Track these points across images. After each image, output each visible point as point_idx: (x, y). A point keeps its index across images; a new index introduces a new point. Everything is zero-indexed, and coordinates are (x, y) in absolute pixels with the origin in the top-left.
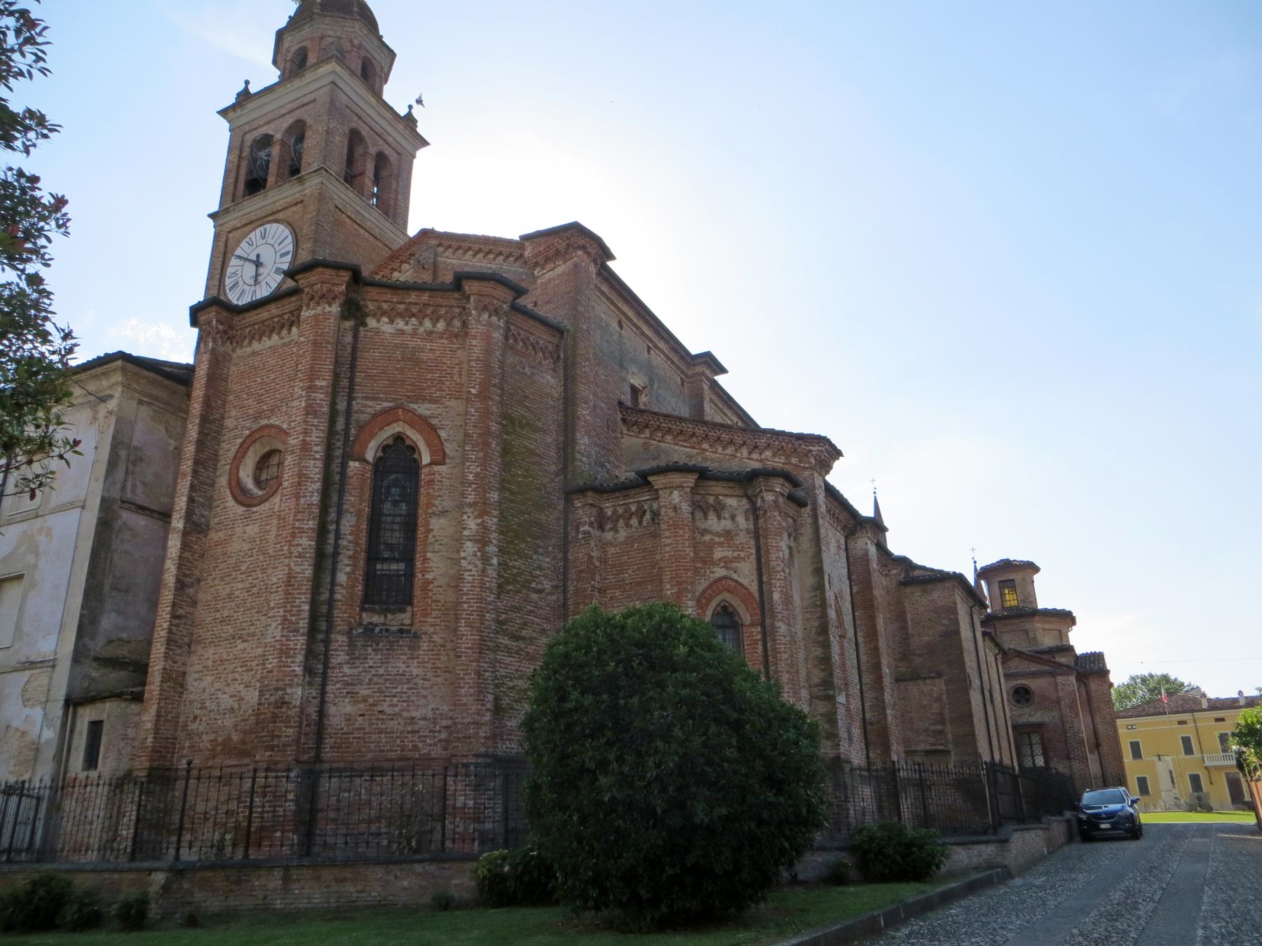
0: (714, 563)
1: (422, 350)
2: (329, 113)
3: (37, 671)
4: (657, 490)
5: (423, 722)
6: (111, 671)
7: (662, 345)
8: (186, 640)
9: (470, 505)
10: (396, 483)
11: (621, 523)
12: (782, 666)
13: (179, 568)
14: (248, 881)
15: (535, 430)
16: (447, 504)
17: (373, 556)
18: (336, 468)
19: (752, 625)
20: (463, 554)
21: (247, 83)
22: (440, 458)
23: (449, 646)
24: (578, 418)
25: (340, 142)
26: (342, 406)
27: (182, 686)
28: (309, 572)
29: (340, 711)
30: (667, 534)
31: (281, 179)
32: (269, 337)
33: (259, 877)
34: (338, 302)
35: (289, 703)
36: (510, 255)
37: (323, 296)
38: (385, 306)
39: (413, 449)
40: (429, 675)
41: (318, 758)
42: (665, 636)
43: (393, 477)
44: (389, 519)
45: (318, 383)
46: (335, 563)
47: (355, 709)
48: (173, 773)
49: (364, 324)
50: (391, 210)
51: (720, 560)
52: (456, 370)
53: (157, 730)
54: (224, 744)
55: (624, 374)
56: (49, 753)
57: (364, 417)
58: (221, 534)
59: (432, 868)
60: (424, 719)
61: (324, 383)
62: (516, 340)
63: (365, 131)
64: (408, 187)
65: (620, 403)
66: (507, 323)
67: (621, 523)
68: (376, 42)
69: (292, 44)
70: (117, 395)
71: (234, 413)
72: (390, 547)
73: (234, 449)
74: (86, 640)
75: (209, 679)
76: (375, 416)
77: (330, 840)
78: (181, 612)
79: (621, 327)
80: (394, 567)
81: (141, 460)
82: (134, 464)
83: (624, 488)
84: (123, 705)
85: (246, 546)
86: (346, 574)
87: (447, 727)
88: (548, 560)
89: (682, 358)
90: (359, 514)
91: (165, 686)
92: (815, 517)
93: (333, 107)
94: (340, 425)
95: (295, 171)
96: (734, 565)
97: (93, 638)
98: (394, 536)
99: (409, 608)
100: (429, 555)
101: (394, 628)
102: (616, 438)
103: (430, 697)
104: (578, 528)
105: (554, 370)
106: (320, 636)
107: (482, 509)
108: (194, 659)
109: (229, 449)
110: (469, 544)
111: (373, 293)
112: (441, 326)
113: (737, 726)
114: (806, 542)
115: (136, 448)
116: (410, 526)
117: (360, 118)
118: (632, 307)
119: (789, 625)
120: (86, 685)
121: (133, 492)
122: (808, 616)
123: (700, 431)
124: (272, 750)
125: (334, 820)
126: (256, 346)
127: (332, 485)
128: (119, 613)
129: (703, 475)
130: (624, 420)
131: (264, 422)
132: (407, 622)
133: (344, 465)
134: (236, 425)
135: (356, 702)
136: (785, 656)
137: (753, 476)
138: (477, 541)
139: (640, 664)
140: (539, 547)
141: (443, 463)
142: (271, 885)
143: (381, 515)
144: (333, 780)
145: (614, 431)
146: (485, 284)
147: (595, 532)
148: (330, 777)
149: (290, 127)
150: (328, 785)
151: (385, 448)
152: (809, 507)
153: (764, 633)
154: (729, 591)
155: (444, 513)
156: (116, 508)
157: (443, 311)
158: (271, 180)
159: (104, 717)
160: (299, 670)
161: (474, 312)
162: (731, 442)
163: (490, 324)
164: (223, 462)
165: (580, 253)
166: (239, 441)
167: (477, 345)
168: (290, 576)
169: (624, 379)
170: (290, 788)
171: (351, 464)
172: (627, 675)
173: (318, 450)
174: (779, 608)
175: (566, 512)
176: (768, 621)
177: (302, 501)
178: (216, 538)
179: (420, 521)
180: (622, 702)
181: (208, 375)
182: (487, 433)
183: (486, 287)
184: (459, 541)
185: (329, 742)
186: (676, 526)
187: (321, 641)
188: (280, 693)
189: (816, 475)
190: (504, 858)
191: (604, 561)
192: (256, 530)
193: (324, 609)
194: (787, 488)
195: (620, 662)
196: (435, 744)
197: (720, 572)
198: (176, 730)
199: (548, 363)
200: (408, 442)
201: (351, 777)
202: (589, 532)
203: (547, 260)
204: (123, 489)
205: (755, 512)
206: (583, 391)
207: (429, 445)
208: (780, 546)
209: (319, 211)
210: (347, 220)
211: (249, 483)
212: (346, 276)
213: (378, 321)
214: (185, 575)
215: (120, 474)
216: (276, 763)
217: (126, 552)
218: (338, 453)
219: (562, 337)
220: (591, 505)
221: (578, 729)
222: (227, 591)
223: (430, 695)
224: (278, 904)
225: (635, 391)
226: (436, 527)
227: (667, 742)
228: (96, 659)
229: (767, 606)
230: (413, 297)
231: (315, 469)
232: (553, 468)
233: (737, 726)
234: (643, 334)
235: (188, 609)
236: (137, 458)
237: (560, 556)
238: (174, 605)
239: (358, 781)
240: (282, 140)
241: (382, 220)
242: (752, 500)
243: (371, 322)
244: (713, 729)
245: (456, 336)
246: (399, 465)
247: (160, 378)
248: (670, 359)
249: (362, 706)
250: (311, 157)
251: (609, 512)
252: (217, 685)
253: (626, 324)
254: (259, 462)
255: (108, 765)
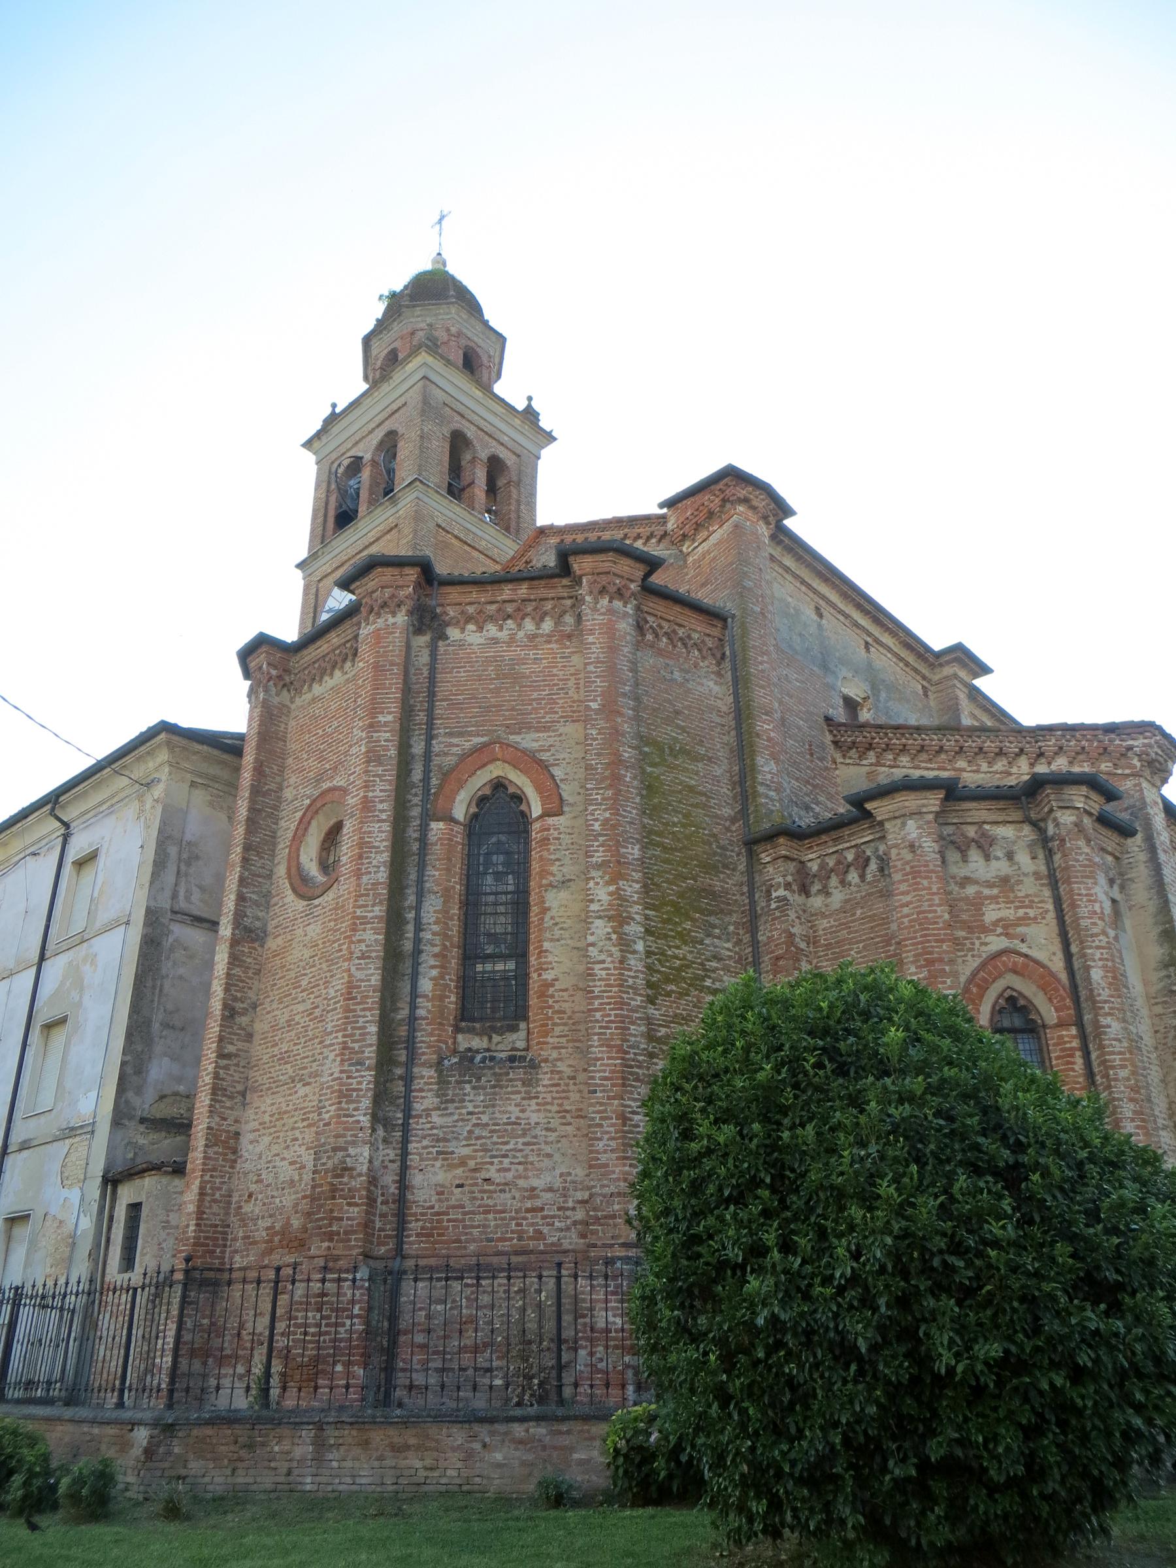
0: (985, 930)
1: (522, 661)
2: (423, 413)
3: (77, 1139)
4: (881, 823)
5: (549, 1195)
6: (153, 1135)
7: (887, 639)
8: (240, 1088)
9: (598, 866)
10: (499, 848)
11: (834, 881)
12: (1120, 1090)
13: (227, 990)
14: (263, 1445)
15: (697, 758)
16: (569, 870)
17: (470, 955)
18: (412, 833)
19: (1061, 1025)
20: (591, 939)
21: (334, 406)
22: (555, 807)
23: (581, 1077)
24: (758, 735)
25: (439, 450)
26: (418, 748)
27: (235, 1151)
28: (376, 980)
29: (429, 1181)
30: (903, 887)
31: (373, 503)
32: (331, 675)
33: (280, 1439)
34: (404, 609)
35: (352, 1169)
36: (652, 536)
37: (384, 605)
38: (471, 610)
39: (519, 798)
40: (555, 1123)
41: (399, 1252)
42: (866, 1015)
43: (494, 840)
44: (491, 898)
45: (381, 718)
46: (416, 965)
47: (450, 1176)
48: (226, 1276)
49: (443, 637)
50: (513, 525)
51: (996, 923)
52: (571, 683)
53: (200, 1213)
54: (283, 1233)
55: (830, 679)
56: (85, 1247)
57: (450, 761)
58: (279, 941)
59: (540, 1431)
60: (550, 1190)
61: (390, 718)
62: (657, 636)
63: (471, 432)
64: (532, 494)
65: (828, 719)
66: (638, 608)
67: (834, 881)
68: (480, 327)
69: (380, 350)
70: (164, 778)
71: (292, 780)
72: (493, 937)
73: (293, 827)
74: (130, 1095)
75: (266, 1140)
76: (463, 757)
77: (419, 1379)
78: (230, 1049)
79: (821, 616)
80: (500, 967)
81: (197, 858)
82: (188, 864)
83: (835, 827)
84: (165, 1180)
85: (307, 953)
86: (433, 981)
87: (583, 1202)
88: (729, 945)
89: (920, 656)
90: (447, 893)
91: (210, 1151)
92: (1152, 849)
93: (427, 407)
94: (417, 775)
95: (388, 491)
96: (1020, 930)
97: (139, 1091)
98: (498, 923)
99: (523, 1025)
100: (546, 945)
101: (503, 1055)
102: (827, 769)
103: (557, 1157)
104: (769, 893)
105: (719, 674)
106: (399, 1071)
107: (616, 871)
108: (250, 1113)
109: (288, 826)
110: (599, 923)
111: (454, 594)
112: (548, 625)
113: (1012, 1177)
114: (1141, 892)
115: (189, 843)
116: (520, 906)
117: (462, 416)
118: (834, 586)
119: (1124, 1021)
120: (131, 1155)
121: (187, 899)
122: (1158, 1009)
123: (950, 743)
124: (331, 1240)
125: (424, 1346)
126: (317, 689)
127: (405, 858)
128: (174, 1059)
129: (952, 792)
130: (835, 743)
131: (326, 785)
132: (521, 1044)
133: (424, 829)
134: (296, 793)
135: (452, 1166)
136: (1123, 1073)
137: (1036, 786)
138: (610, 918)
139: (819, 1065)
140: (714, 926)
141: (560, 813)
142: (298, 1452)
143: (479, 894)
144: (420, 1284)
145: (822, 759)
146: (602, 557)
147: (796, 899)
148: (416, 1280)
149: (381, 443)
150: (414, 1292)
151: (482, 801)
152: (1139, 836)
153: (1083, 1037)
154: (1015, 972)
155: (565, 883)
156: (165, 921)
157: (549, 606)
158: (362, 509)
159: (142, 1198)
160: (365, 1120)
161: (588, 598)
162: (1000, 753)
163: (611, 611)
164: (281, 846)
165: (741, 508)
166: (299, 814)
167: (595, 642)
168: (351, 986)
169: (832, 687)
170: (353, 1294)
171: (434, 825)
172: (796, 1086)
173: (385, 809)
174: (1104, 994)
175: (750, 872)
176: (1087, 1017)
177: (365, 879)
178: (274, 947)
179: (533, 898)
180: (786, 1135)
181: (259, 733)
182: (617, 761)
183: (604, 562)
184: (585, 921)
185: (414, 1226)
186: (915, 873)
187: (401, 1078)
188: (340, 1154)
189: (1145, 784)
190: (652, 1419)
191: (812, 940)
192: (318, 930)
193: (403, 1032)
194: (1096, 804)
195: (783, 1064)
196: (568, 1229)
197: (997, 943)
198: (227, 1214)
199: (708, 664)
200: (511, 790)
201: (447, 1279)
202: (785, 899)
203: (698, 527)
204: (174, 896)
205: (1045, 844)
206: (761, 696)
207: (539, 789)
208: (1095, 896)
209: (415, 532)
210: (454, 541)
211: (312, 868)
212: (412, 574)
213: (463, 630)
214: (235, 999)
215: (169, 877)
216: (337, 1259)
217: (181, 977)
218: (415, 812)
219: (725, 627)
220: (786, 857)
221: (711, 1189)
222: (286, 1017)
223: (549, 1156)
224: (308, 1484)
225: (851, 705)
226: (555, 904)
227: (870, 1209)
228: (143, 1120)
229: (1083, 994)
230: (507, 592)
231: (380, 833)
232: (727, 811)
233: (1012, 1177)
234: (856, 625)
235: (240, 1045)
236: (190, 855)
237: (746, 938)
238: (221, 1039)
239: (456, 1286)
240: (373, 460)
241: (500, 537)
242: (1037, 825)
243: (453, 633)
244: (962, 1181)
245: (569, 637)
246: (501, 823)
247: (216, 752)
248: (901, 659)
249: (459, 1171)
250: (405, 472)
251: (814, 867)
252: (275, 1149)
253: (826, 610)
254: (324, 841)
255: (145, 1259)
